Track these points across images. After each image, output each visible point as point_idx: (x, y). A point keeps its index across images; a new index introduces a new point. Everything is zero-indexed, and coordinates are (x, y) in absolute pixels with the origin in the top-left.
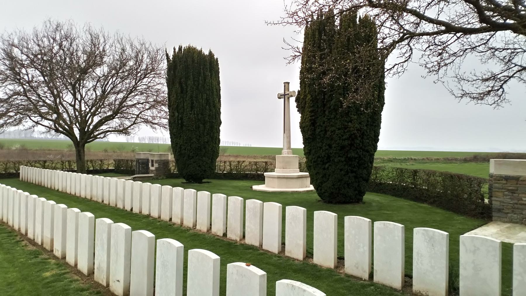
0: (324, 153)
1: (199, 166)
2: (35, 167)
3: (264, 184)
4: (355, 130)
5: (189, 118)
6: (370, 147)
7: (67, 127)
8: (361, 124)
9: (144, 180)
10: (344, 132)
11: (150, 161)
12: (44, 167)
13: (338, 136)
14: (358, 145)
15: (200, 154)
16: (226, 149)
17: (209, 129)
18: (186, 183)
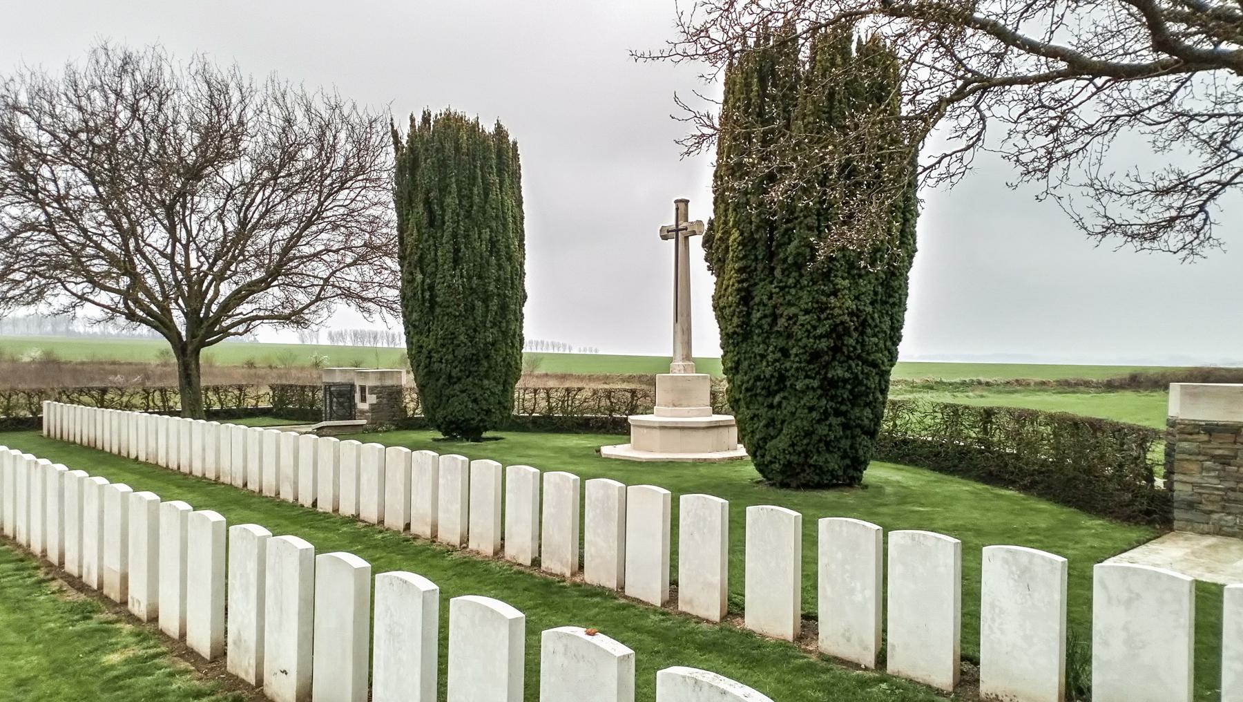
3: (629, 441)
4: (844, 314)
5: (449, 287)
7: (155, 309)
9: (342, 433)
11: (358, 389)
12: (102, 404)
17: (496, 313)
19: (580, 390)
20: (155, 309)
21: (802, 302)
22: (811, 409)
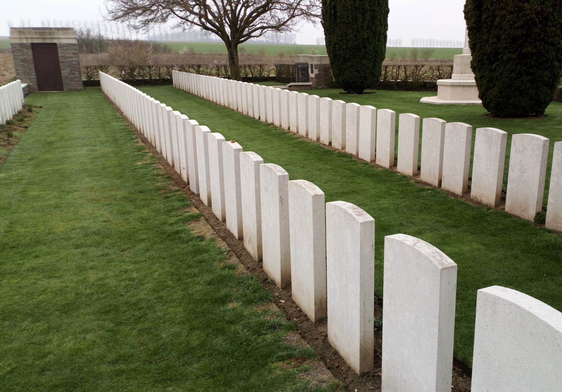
0: (490, 47)
1: (358, 72)
2: (189, 72)
3: (436, 95)
4: (532, 14)
5: (344, 6)
6: (557, 38)
7: (217, 24)
8: (544, 4)
9: (300, 89)
10: (518, 17)
11: (310, 66)
12: (198, 72)
13: (509, 24)
14: (537, 35)
15: (359, 55)
16: (390, 48)
17: (369, 21)
18: (346, 93)
19: (423, 66)
20: (217, 24)
21: (509, 7)
22: (511, 71)
